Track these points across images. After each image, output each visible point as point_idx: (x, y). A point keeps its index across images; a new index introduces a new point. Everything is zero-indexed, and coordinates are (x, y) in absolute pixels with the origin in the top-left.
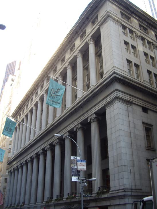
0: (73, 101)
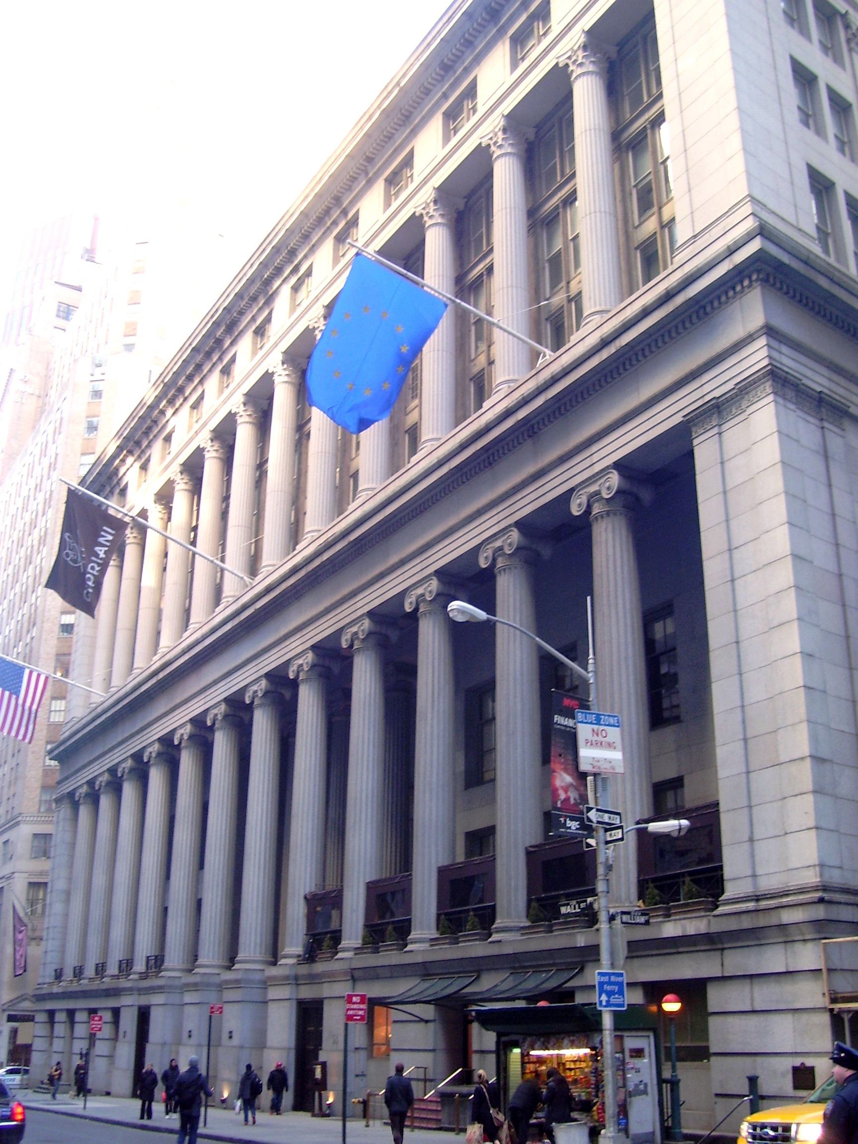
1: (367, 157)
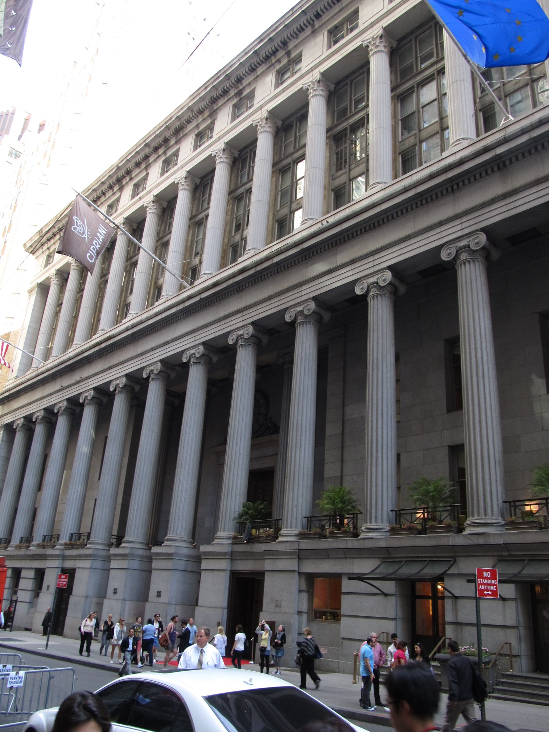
0: (117, 321)
1: (146, 155)
